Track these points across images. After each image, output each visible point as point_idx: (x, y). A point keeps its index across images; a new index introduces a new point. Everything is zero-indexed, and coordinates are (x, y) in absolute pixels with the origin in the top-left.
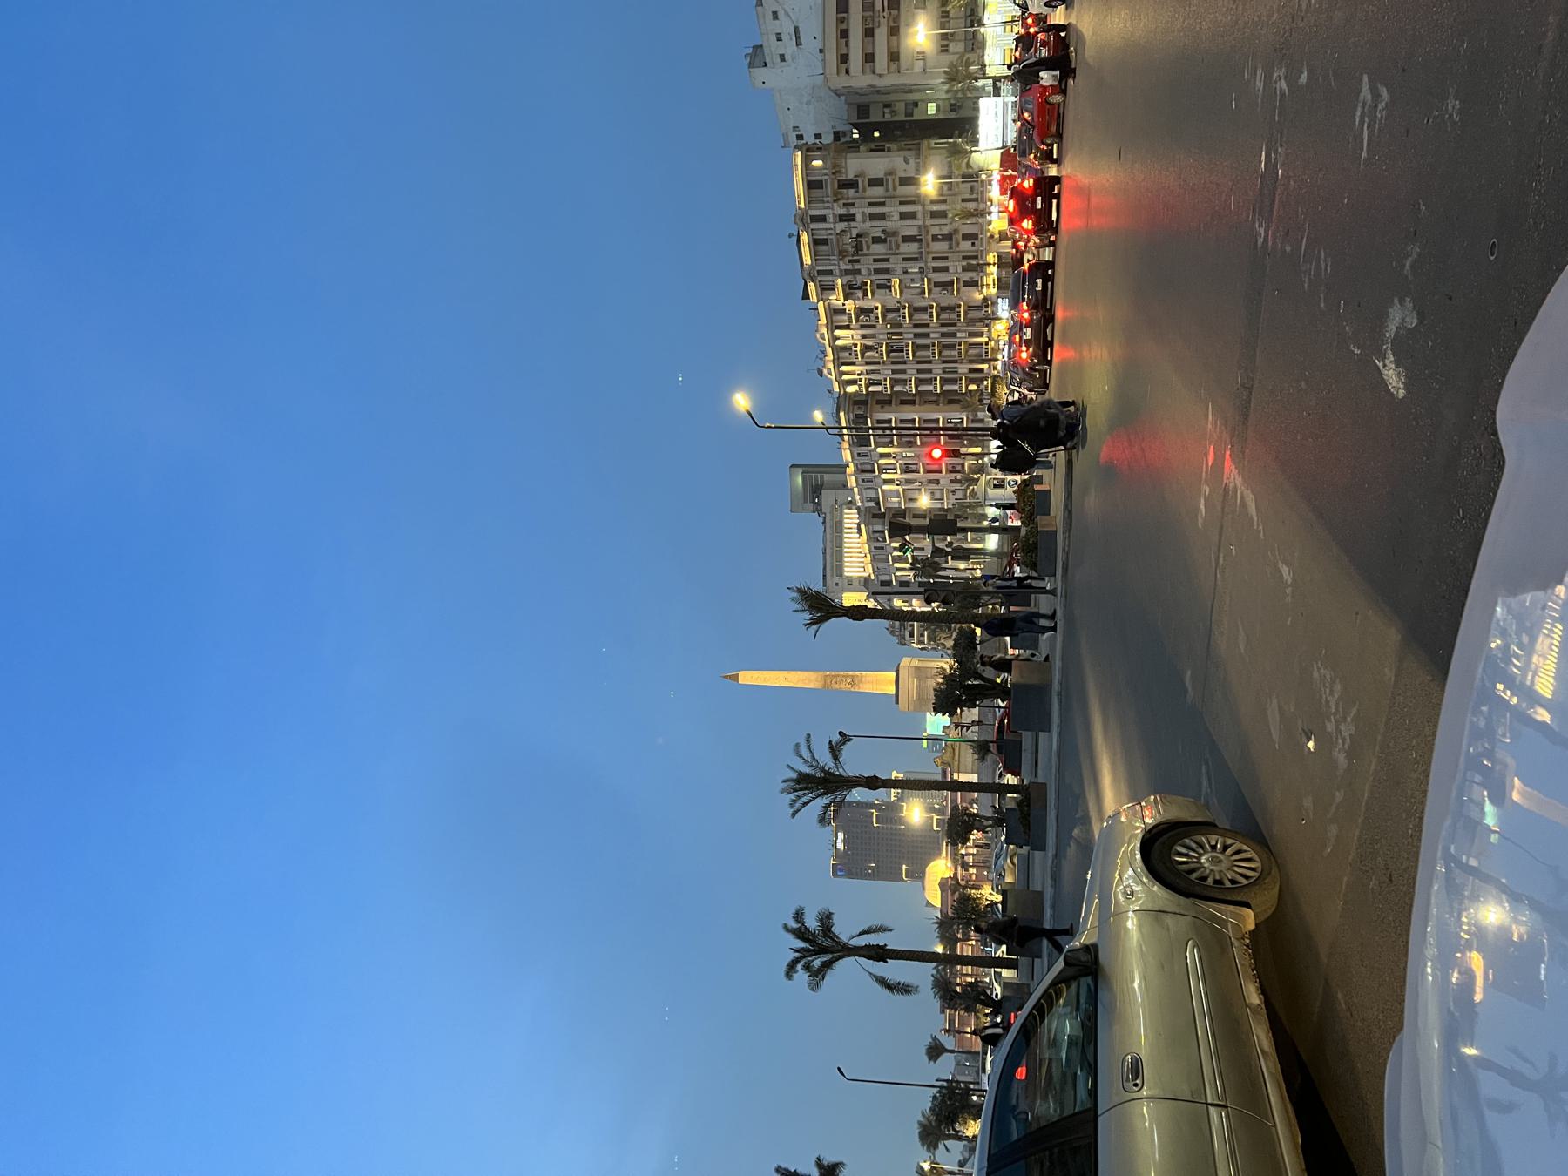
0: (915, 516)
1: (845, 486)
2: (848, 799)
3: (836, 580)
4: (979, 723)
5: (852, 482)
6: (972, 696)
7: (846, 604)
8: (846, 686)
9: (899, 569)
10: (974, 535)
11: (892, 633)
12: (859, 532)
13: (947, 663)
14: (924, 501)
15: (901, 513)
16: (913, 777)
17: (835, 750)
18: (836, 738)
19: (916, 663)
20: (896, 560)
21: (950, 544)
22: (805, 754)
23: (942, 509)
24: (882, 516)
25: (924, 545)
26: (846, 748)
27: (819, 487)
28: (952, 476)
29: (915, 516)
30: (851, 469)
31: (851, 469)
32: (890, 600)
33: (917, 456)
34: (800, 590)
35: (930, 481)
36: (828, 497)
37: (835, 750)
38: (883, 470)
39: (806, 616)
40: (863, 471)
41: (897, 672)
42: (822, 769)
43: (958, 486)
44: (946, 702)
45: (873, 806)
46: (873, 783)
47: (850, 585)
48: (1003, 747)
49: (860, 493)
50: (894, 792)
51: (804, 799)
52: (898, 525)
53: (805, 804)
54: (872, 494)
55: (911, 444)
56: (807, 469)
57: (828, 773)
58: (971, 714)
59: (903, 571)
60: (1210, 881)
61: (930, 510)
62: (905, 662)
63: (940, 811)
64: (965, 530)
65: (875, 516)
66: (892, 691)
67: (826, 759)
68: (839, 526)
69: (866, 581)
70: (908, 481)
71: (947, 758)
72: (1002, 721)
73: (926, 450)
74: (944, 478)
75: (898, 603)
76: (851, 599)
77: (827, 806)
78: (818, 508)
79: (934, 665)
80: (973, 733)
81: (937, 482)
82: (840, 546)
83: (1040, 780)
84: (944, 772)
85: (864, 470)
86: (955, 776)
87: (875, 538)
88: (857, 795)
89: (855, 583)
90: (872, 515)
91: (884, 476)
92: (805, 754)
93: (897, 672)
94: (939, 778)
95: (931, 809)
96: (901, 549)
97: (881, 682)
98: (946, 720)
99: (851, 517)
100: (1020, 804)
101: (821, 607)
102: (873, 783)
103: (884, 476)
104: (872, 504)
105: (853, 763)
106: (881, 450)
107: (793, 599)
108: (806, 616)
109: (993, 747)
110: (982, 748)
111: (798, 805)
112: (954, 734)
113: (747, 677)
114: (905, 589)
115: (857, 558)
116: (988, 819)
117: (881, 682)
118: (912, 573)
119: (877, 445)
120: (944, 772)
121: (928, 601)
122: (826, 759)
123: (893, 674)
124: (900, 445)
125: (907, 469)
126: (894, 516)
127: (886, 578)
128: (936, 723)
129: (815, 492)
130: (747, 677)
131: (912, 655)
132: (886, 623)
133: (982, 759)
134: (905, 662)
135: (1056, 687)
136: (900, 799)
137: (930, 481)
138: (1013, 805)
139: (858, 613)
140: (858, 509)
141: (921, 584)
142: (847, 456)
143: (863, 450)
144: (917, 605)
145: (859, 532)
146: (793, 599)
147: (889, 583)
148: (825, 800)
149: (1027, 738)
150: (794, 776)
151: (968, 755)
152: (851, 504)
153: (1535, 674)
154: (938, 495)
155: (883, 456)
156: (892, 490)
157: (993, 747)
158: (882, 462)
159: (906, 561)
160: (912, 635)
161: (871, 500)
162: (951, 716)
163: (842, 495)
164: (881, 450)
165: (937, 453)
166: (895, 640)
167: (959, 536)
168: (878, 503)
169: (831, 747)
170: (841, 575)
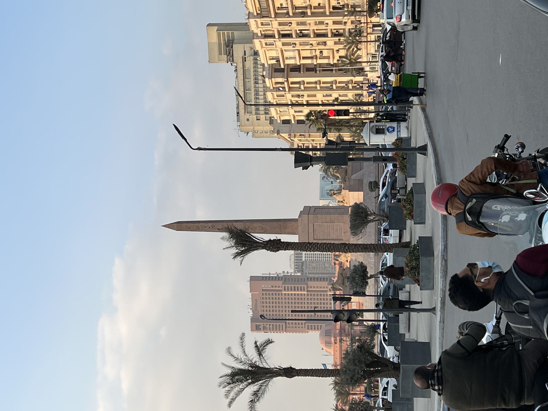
56: (222, 27)
108: (234, 251)
111: (232, 395)
127: (287, 118)
148: (254, 388)
168: (278, 61)
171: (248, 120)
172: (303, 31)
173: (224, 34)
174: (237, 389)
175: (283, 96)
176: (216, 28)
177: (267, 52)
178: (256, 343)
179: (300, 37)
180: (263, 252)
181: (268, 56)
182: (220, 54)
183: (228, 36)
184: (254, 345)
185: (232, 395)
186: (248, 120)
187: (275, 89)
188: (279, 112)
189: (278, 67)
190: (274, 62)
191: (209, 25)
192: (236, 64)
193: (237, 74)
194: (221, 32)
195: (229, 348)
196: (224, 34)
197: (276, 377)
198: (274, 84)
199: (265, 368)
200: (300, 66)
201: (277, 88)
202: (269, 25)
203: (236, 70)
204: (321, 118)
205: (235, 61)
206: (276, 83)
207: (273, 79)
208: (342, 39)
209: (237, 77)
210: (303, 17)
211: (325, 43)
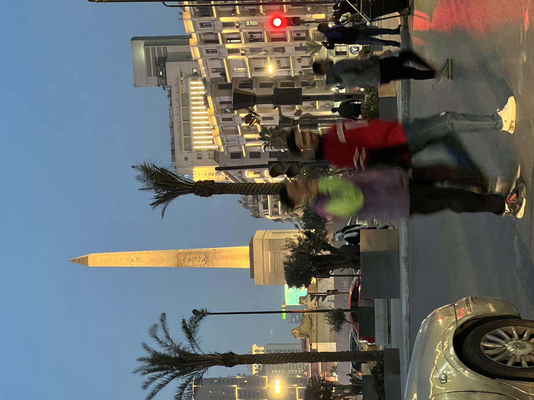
0: (263, 85)
1: (188, 57)
2: (205, 376)
3: (185, 154)
4: (335, 292)
5: (196, 53)
6: (323, 268)
7: (196, 179)
8: (198, 263)
9: (248, 140)
10: (323, 103)
11: (246, 205)
12: (206, 104)
13: (296, 234)
14: (271, 70)
15: (248, 83)
16: (274, 350)
17: (189, 331)
18: (189, 316)
19: (269, 235)
20: (244, 131)
21: (299, 113)
22: (161, 334)
23: (290, 77)
24: (229, 87)
25: (269, 115)
26: (205, 323)
27: (163, 58)
28: (298, 43)
29: (263, 85)
30: (194, 40)
31: (194, 40)
32: (240, 172)
33: (261, 25)
34: (145, 169)
35: (276, 50)
36: (172, 69)
37: (189, 331)
38: (228, 39)
39: (152, 195)
40: (207, 42)
41: (251, 246)
42: (177, 350)
43: (303, 53)
44: (297, 275)
45: (233, 381)
46: (229, 360)
47: (200, 158)
48: (359, 315)
49: (205, 64)
50: (255, 366)
51: (159, 381)
52: (239, 96)
53: (161, 386)
54: (217, 64)
55: (254, 13)
56: (150, 42)
57: (183, 353)
58: (328, 283)
59: (252, 141)
60: (524, 364)
61: (276, 79)
62: (259, 234)
63: (299, 381)
64: (308, 98)
65: (221, 87)
66: (246, 264)
67: (180, 339)
68: (185, 99)
69: (216, 155)
70: (253, 51)
71: (305, 328)
72: (355, 289)
73: (270, 17)
74: (290, 45)
75: (249, 175)
76: (202, 173)
77: (183, 387)
78: (163, 81)
79: (284, 236)
80: (329, 303)
81: (283, 50)
82: (187, 119)
83: (394, 347)
84: (304, 342)
85: (209, 41)
86: (314, 346)
87: (221, 110)
88: (215, 372)
89: (205, 156)
90: (218, 85)
91: (229, 46)
92: (161, 334)
93: (251, 246)
94: (299, 349)
95: (293, 380)
96: (248, 119)
97: (237, 257)
98: (303, 291)
99: (197, 88)
100: (374, 371)
101: (167, 185)
102: (229, 360)
103: (229, 46)
104: (218, 75)
105: (210, 340)
106: (224, 19)
107: (138, 178)
108: (152, 195)
109: (348, 316)
110: (337, 318)
111: (152, 387)
112: (312, 304)
113: (98, 260)
114: (254, 160)
115: (205, 128)
116: (345, 387)
117: (237, 257)
118: (261, 143)
119: (220, 14)
120: (304, 342)
121: (273, 174)
122: (180, 339)
123: (247, 248)
124: (243, 14)
125: (251, 39)
126: (241, 86)
127: (235, 150)
128: (293, 296)
129: (160, 64)
130: (98, 260)
131: (266, 226)
132: (239, 197)
133: (338, 328)
134: (259, 234)
135: (403, 253)
136: (262, 372)
137: (276, 50)
138: (369, 373)
139: (206, 189)
140: (204, 80)
141: (272, 155)
142: (189, 26)
143: (206, 20)
144: (264, 177)
145: (206, 104)
146: (138, 178)
147: (237, 155)
148: (180, 381)
149: (379, 305)
150: (149, 355)
151: (324, 325)
152: (196, 76)
153: (154, 166)
154: (284, 63)
155: (226, 25)
156: (238, 62)
157: (348, 316)
158: (226, 31)
159: (256, 131)
160: (265, 207)
161: (216, 70)
162: (307, 286)
163: (185, 66)
164: (224, 19)
165: (277, 22)
166: (249, 213)
167: (305, 104)
168: (224, 74)
169: (185, 327)
170: (189, 148)
171: (186, 159)
172: (254, 35)
173: (153, 50)
174: (159, 381)
175: (231, 119)
176: (142, 43)
177: (209, 62)
178: (184, 322)
179: (251, 41)
180: (191, 197)
181: (210, 68)
182: (149, 75)
183: (159, 52)
184: (181, 325)
185: (152, 387)
186: (186, 159)
187: (220, 111)
188: (225, 142)
189: (225, 83)
190: (218, 75)
191: (134, 39)
192: (169, 88)
193: (171, 101)
194: (150, 47)
195: (132, 166)
196: (153, 50)
197: (211, 366)
198: (218, 104)
199: (198, 355)
200: (251, 80)
201: (222, 109)
202: (210, 25)
203: (170, 96)
204: (280, 136)
205: (168, 84)
206: (222, 103)
207: (217, 98)
208: (304, 44)
209: (171, 104)
210: (254, 15)
211: (283, 50)
